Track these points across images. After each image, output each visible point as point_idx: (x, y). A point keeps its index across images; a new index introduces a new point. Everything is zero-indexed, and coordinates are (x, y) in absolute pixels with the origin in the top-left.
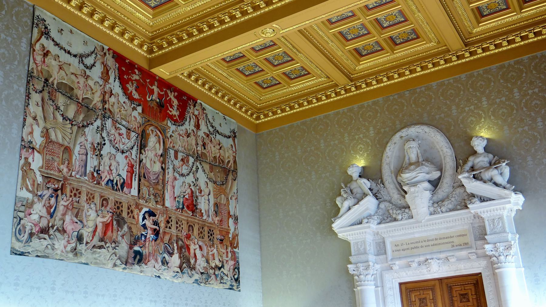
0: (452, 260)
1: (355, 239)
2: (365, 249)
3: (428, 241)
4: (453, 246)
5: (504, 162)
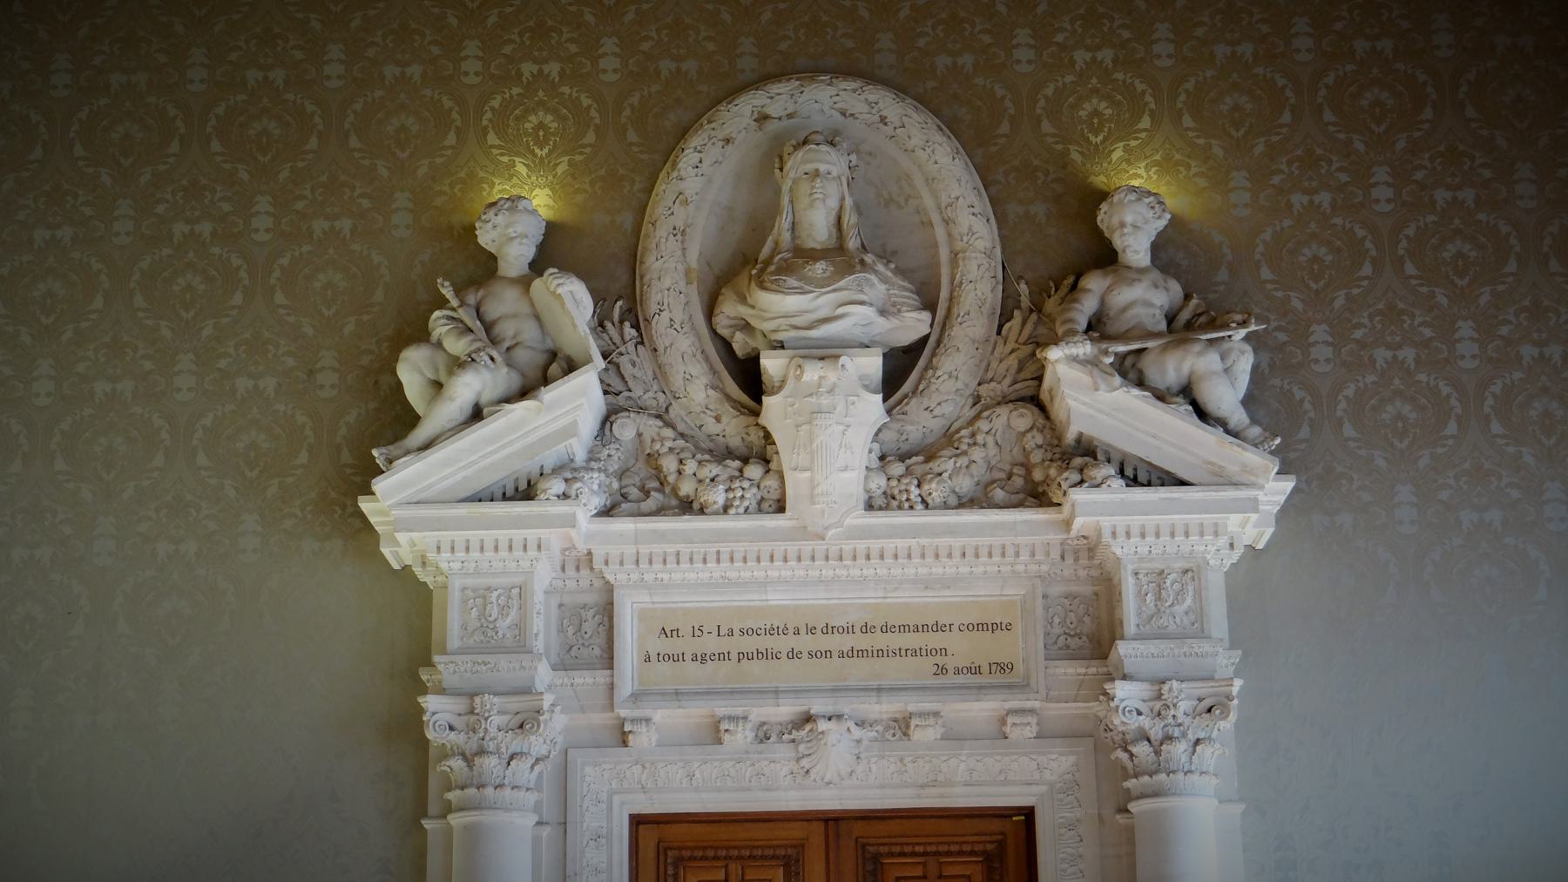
0: (926, 734)
1: (477, 573)
2: (521, 627)
3: (828, 630)
5: (1243, 324)
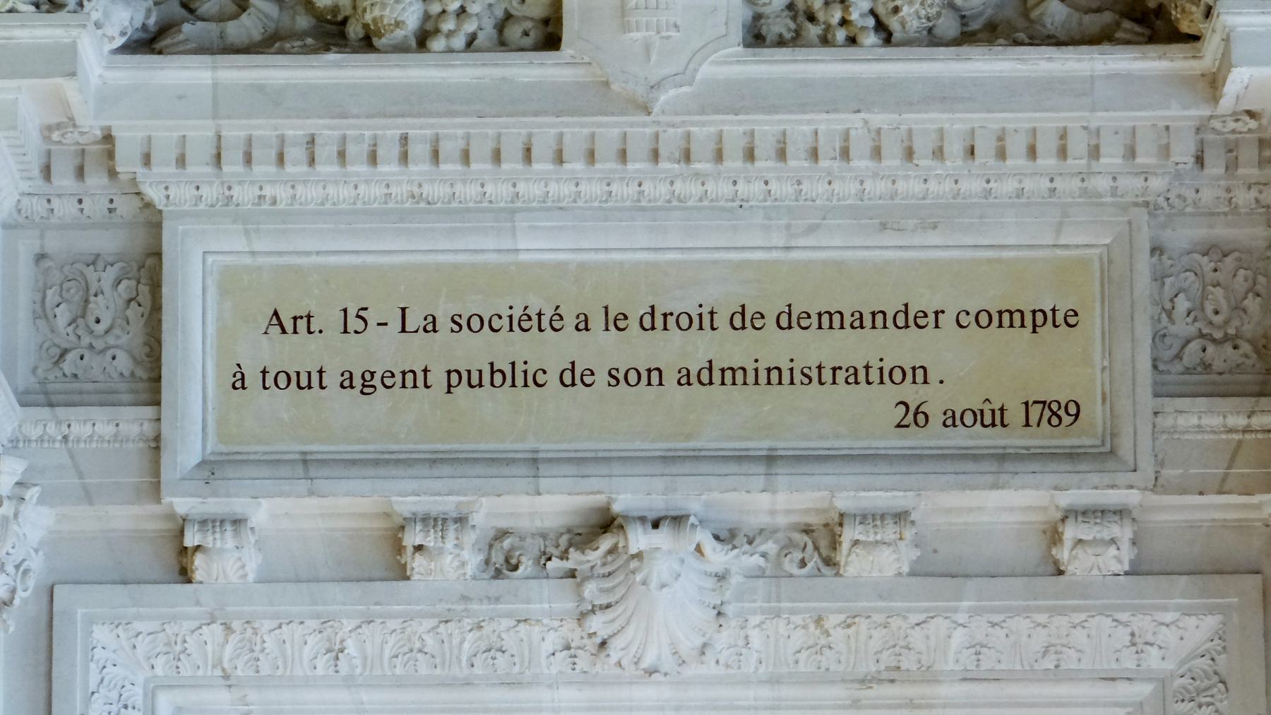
3: (654, 320)
4: (915, 416)
